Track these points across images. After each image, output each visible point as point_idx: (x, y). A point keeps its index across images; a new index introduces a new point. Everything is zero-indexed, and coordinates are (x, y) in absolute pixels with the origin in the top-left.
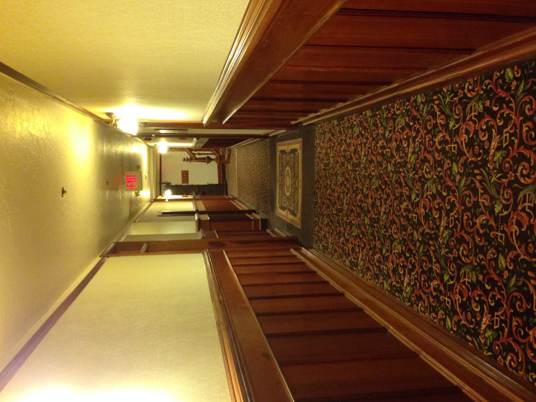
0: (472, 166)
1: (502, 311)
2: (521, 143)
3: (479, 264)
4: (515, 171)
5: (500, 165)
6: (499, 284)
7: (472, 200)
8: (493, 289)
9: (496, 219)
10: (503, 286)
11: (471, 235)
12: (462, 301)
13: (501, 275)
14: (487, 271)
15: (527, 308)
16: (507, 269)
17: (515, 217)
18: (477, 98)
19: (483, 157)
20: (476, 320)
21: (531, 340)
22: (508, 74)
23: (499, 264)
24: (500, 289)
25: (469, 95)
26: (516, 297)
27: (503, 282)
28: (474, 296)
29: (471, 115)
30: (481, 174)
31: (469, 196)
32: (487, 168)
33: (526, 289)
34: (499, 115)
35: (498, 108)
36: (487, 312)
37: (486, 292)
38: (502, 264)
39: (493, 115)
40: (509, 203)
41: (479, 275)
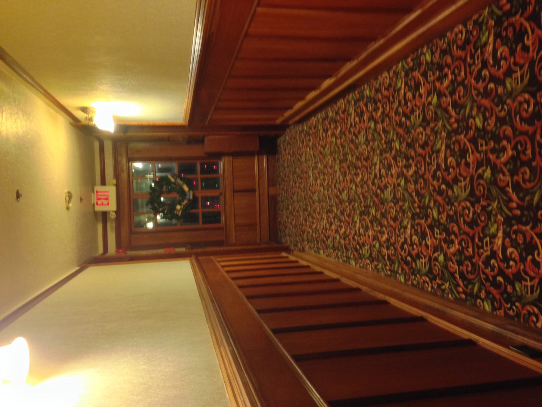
0: (524, 219)
1: (482, 257)
2: (465, 60)
3: (513, 304)
4: (474, 213)
5: (489, 219)
6: (489, 284)
7: (521, 176)
8: (494, 277)
9: (488, 161)
10: (485, 282)
11: (518, 133)
12: (533, 256)
13: (488, 293)
14: (502, 296)
15: (463, 266)
16: (483, 300)
17: (471, 170)
18: (514, 94)
19: (511, 229)
20: (510, 238)
21: (456, 240)
22: (480, 122)
23: (490, 304)
24: (487, 279)
25: (527, 96)
26: (471, 274)
27: (485, 286)
28: (516, 265)
29: (522, 71)
30: (511, 210)
31: (524, 181)
32: (504, 215)
33: (465, 283)
34: (487, 79)
35: (489, 86)
36: (498, 252)
37: (501, 273)
38: (488, 304)
39: (493, 79)
40: (478, 181)
41: (512, 291)
